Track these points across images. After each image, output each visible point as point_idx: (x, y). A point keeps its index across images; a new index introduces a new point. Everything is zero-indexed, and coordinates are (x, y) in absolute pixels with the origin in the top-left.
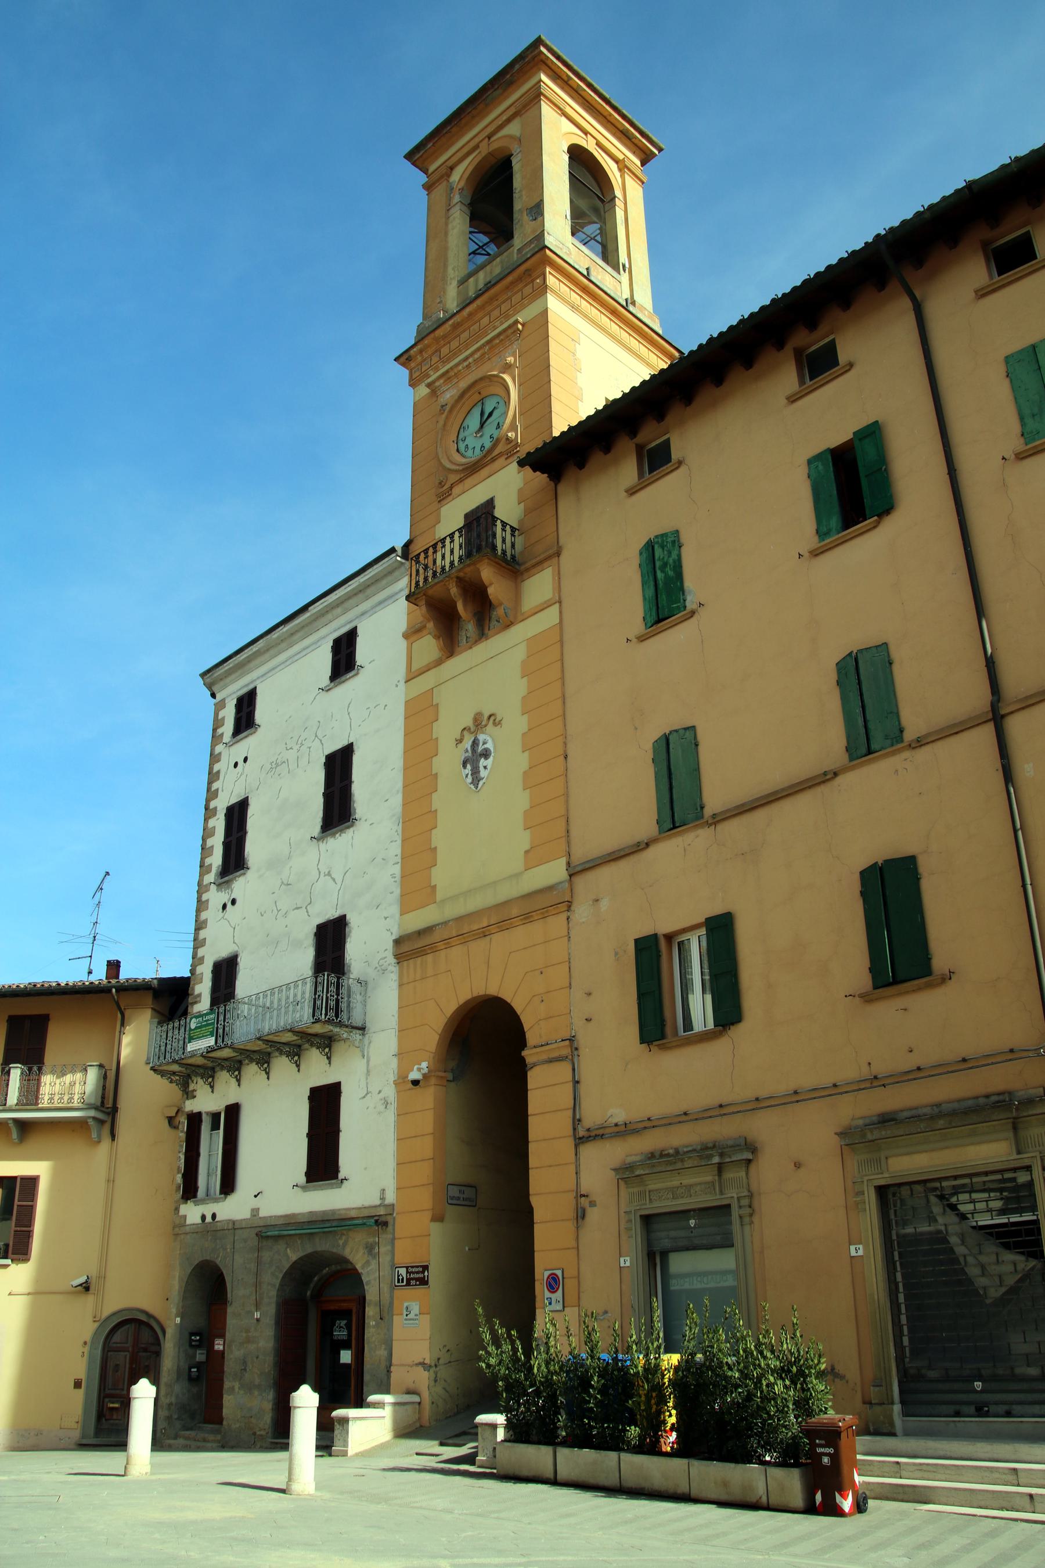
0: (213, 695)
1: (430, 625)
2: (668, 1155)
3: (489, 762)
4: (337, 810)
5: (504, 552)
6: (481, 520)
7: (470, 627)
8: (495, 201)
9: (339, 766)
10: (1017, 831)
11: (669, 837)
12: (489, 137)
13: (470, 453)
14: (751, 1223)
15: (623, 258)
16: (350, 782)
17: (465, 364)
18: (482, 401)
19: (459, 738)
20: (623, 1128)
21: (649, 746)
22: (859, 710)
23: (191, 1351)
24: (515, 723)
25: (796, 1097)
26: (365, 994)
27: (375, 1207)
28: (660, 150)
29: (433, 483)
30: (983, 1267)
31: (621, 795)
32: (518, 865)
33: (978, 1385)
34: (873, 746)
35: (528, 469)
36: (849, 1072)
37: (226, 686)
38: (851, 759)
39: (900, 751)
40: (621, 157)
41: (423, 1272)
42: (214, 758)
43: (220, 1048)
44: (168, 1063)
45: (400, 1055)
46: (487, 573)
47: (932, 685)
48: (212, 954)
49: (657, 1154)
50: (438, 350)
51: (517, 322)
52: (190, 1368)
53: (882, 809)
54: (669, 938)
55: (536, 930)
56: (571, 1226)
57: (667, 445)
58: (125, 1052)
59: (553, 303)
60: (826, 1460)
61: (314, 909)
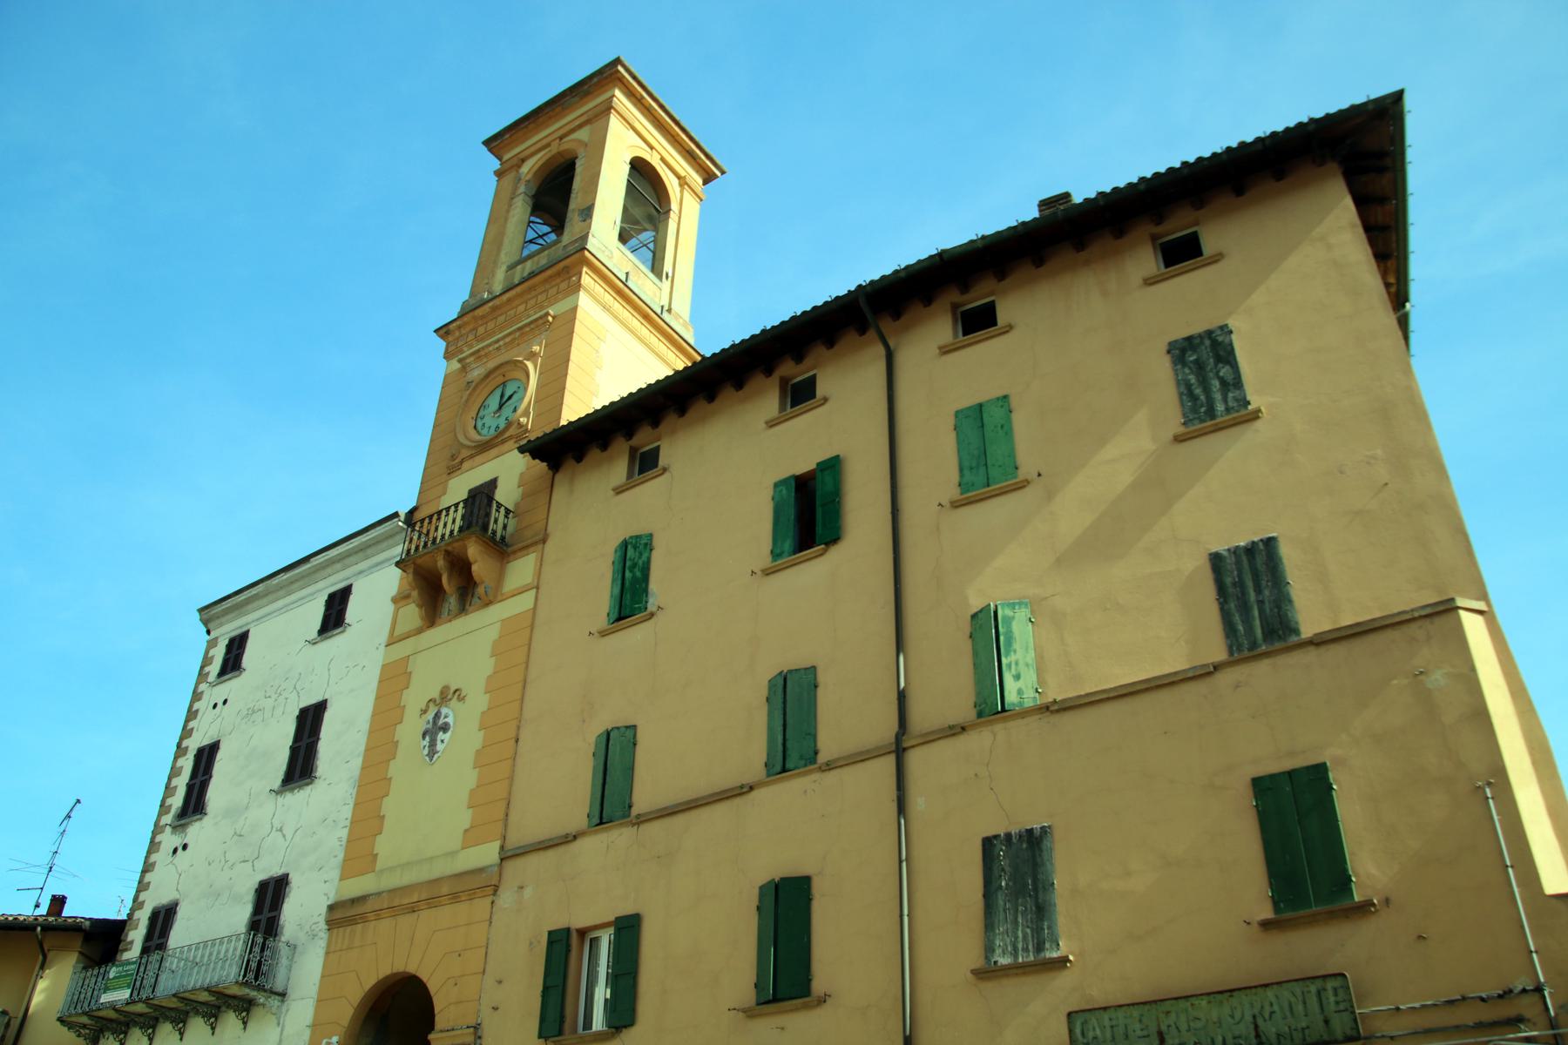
0: (208, 632)
1: (415, 594)
3: (446, 736)
4: (301, 766)
5: (494, 532)
6: (482, 497)
7: (452, 601)
8: (555, 194)
9: (310, 720)
10: (904, 859)
11: (596, 832)
12: (561, 138)
13: (485, 432)
15: (668, 267)
18: (504, 384)
21: (592, 739)
22: (780, 729)
24: (477, 701)
26: (291, 959)
28: (723, 173)
29: (448, 454)
31: (559, 785)
32: (456, 843)
34: (788, 765)
35: (528, 457)
37: (221, 625)
38: (769, 775)
39: (811, 772)
40: (683, 173)
42: (197, 695)
43: (134, 1002)
44: (77, 1014)
45: (314, 1026)
46: (473, 550)
47: (849, 716)
48: (152, 900)
50: (475, 329)
51: (547, 314)
53: (798, 827)
54: (582, 933)
55: (462, 908)
57: (657, 450)
58: (37, 999)
59: (583, 300)
61: (259, 865)
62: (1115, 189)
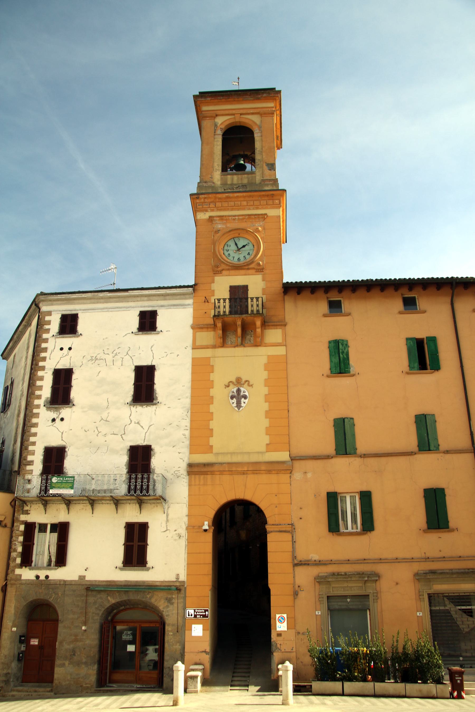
2: (341, 575)
3: (246, 401)
5: (252, 311)
14: (377, 602)
16: (153, 384)
17: (233, 218)
19: (227, 384)
20: (318, 562)
23: (19, 645)
25: (396, 560)
27: (173, 582)
30: (463, 622)
32: (263, 449)
33: (461, 658)
36: (417, 554)
38: (337, 454)
41: (205, 612)
49: (336, 574)
52: (19, 654)
55: (274, 478)
56: (292, 598)
60: (459, 681)
62: (423, 278)
